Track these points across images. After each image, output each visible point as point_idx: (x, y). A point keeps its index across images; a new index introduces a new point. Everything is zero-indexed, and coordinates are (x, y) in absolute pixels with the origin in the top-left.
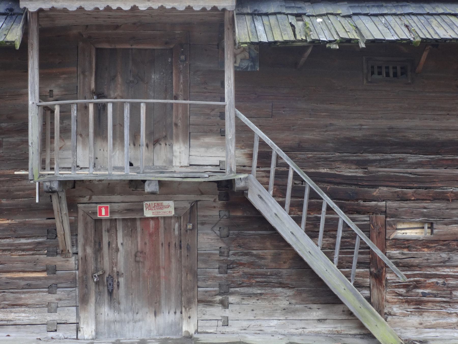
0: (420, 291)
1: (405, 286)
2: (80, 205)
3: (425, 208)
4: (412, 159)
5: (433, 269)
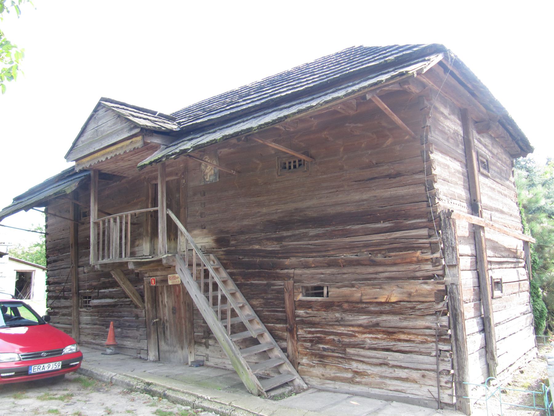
0: (321, 346)
1: (311, 341)
2: (144, 278)
3: (323, 274)
4: (313, 232)
5: (331, 327)
